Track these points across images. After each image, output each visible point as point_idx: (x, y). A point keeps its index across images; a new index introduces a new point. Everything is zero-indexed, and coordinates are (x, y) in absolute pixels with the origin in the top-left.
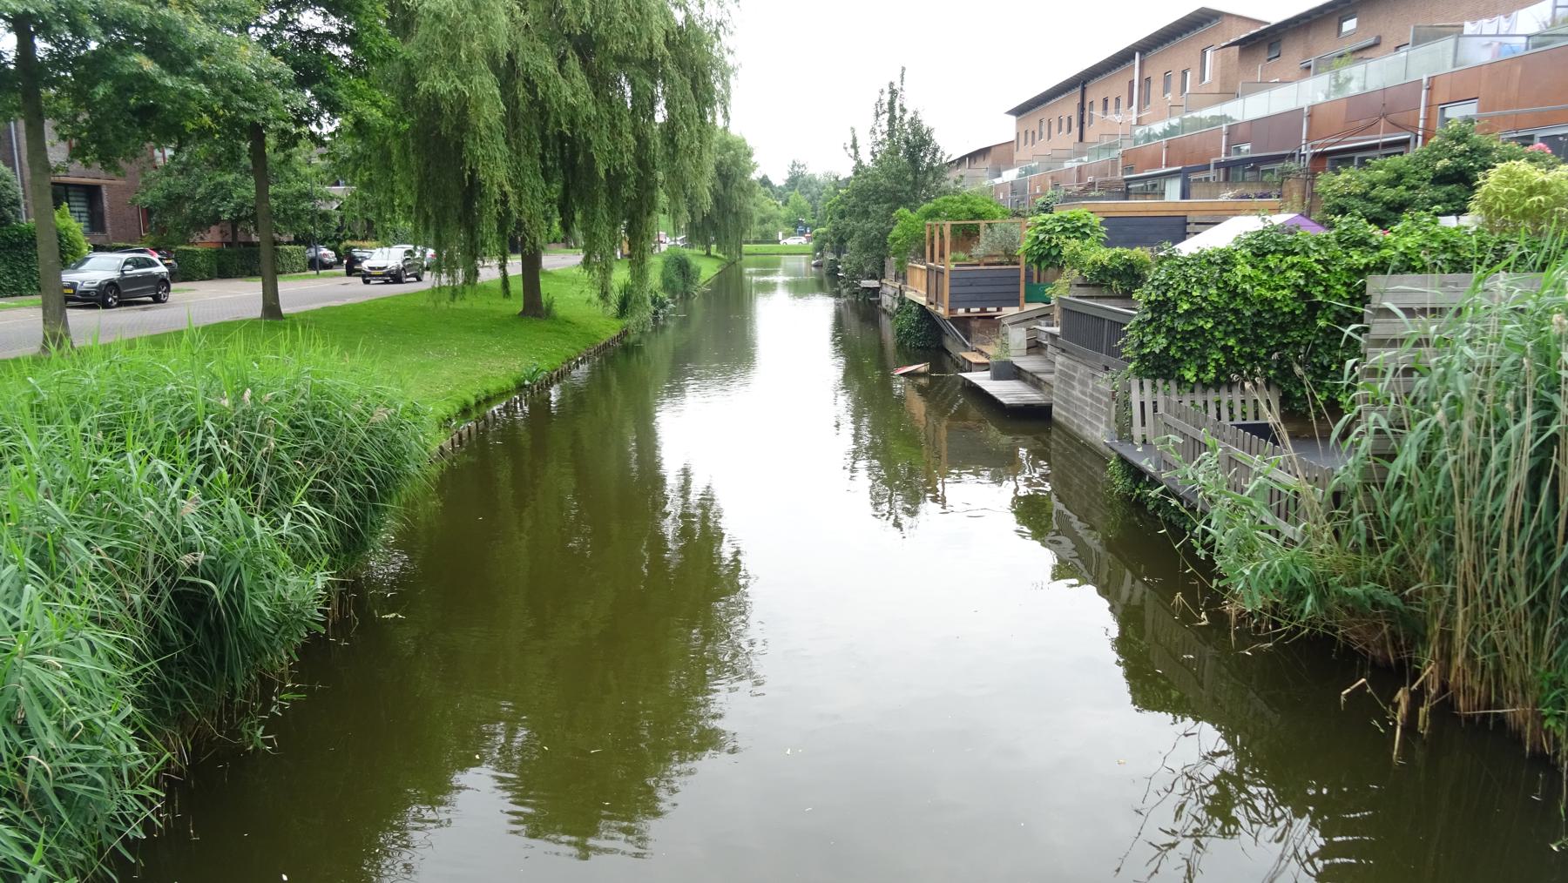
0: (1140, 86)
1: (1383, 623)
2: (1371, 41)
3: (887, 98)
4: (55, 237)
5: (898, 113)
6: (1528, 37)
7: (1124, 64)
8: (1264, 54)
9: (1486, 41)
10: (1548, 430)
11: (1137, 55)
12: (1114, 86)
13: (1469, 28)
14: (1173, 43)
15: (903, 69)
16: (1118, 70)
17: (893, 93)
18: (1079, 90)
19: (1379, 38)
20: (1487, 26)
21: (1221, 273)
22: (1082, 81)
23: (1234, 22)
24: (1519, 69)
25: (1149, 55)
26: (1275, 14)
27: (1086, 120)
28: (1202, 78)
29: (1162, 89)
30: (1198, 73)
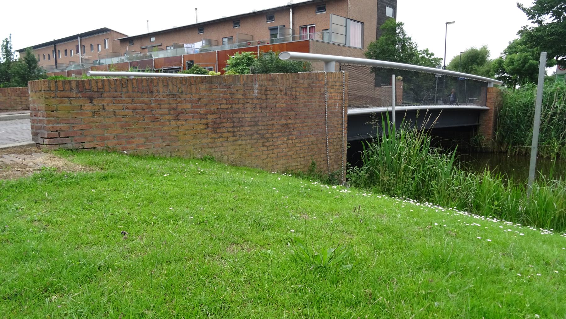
0: (81, 47)
1: (389, 269)
2: (160, 44)
3: (5, 43)
4: (68, 136)
5: (9, 49)
6: (199, 49)
7: (73, 39)
8: (128, 44)
9: (192, 49)
10: (455, 158)
11: (79, 38)
12: (70, 46)
13: (185, 45)
14: (92, 36)
15: (10, 34)
16: (70, 41)
17: (7, 42)
18: (53, 45)
19: (161, 44)
20: (189, 45)
21: (220, 116)
22: (55, 43)
23: (114, 32)
24: (201, 56)
25: (83, 38)
26: (131, 34)
27: (57, 56)
28: (105, 47)
29: (90, 49)
30: (104, 45)
